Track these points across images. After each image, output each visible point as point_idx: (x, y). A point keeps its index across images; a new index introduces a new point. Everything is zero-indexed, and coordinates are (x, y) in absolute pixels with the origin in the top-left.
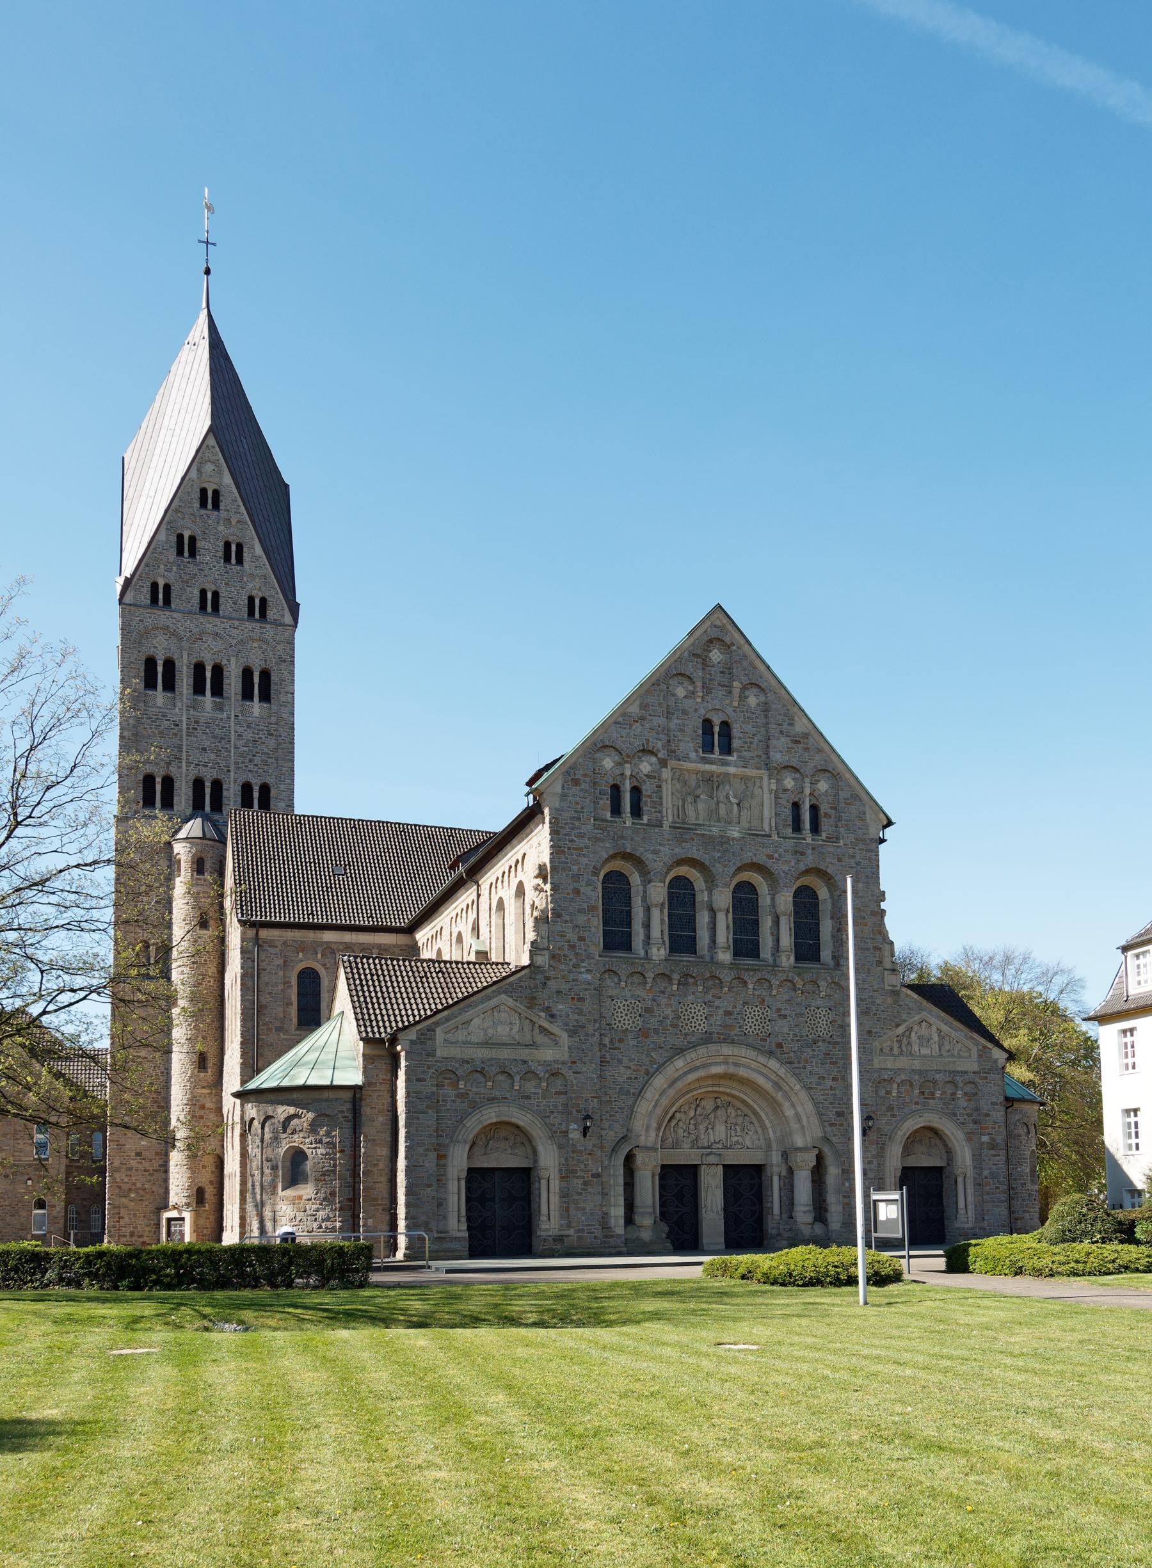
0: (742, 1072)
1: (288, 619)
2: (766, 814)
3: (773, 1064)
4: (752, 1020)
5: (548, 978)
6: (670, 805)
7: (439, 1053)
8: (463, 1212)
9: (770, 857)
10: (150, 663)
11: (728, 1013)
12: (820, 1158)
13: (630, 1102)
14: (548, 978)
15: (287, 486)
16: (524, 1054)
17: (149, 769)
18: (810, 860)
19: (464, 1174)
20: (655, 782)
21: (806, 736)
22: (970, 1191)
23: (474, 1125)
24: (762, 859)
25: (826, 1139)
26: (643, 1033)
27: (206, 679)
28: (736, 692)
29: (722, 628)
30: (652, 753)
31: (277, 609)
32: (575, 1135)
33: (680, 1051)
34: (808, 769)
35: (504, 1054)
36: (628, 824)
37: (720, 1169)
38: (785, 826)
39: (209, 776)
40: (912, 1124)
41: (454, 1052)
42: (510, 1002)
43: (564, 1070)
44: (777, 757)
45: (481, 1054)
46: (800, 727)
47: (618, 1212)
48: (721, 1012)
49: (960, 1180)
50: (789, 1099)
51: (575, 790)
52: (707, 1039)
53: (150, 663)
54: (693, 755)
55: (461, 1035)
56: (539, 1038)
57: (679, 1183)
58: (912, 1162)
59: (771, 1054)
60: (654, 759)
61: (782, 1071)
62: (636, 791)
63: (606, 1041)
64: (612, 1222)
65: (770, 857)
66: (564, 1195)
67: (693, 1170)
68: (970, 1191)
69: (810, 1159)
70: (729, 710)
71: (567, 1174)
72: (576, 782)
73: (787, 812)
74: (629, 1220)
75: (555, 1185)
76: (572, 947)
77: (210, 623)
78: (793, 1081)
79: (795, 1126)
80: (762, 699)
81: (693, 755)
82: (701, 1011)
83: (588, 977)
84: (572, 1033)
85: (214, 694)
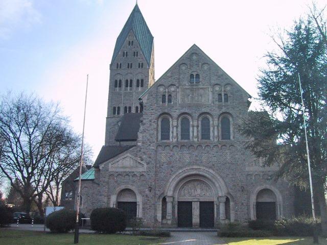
0: (201, 173)
1: (148, 67)
2: (210, 98)
3: (211, 171)
4: (204, 159)
5: (141, 149)
6: (180, 98)
7: (110, 170)
8: (255, 214)
9: (211, 110)
10: (116, 81)
11: (196, 156)
12: (227, 199)
13: (165, 183)
14: (141, 149)
15: (152, 38)
16: (133, 170)
17: (114, 106)
18: (224, 110)
19: (255, 204)
20: (175, 93)
21: (222, 75)
22: (282, 209)
23: (118, 189)
24: (208, 111)
25: (229, 193)
26: (169, 163)
27: (129, 83)
28: (200, 66)
29: (196, 50)
30: (174, 85)
31: (145, 65)
32: (147, 192)
33: (181, 168)
34: (223, 84)
35: (127, 170)
36: (166, 105)
37: (199, 203)
38: (216, 101)
39: (128, 106)
40: (259, 188)
41: (114, 170)
42: (130, 156)
43: (145, 174)
44: (213, 82)
45: (122, 170)
46: (220, 73)
47: (159, 215)
48: (194, 156)
49: (278, 206)
50: (216, 181)
51: (151, 97)
52: (190, 164)
53: (116, 81)
54: (187, 84)
55: (116, 165)
56: (138, 165)
57: (184, 208)
58: (260, 200)
59: (210, 168)
60: (175, 87)
61: (214, 173)
62: (170, 95)
63: (158, 165)
64: (158, 218)
65: (211, 110)
66: (143, 208)
67: (191, 203)
68: (282, 209)
69: (224, 200)
70: (199, 71)
71: (144, 204)
72: (152, 95)
73: (217, 97)
74: (164, 217)
75: (141, 207)
76: (148, 140)
77: (130, 71)
78: (217, 175)
79: (219, 190)
80: (209, 67)
81: (187, 84)
82: (188, 156)
83: (153, 148)
84: (148, 163)
85: (141, 87)
